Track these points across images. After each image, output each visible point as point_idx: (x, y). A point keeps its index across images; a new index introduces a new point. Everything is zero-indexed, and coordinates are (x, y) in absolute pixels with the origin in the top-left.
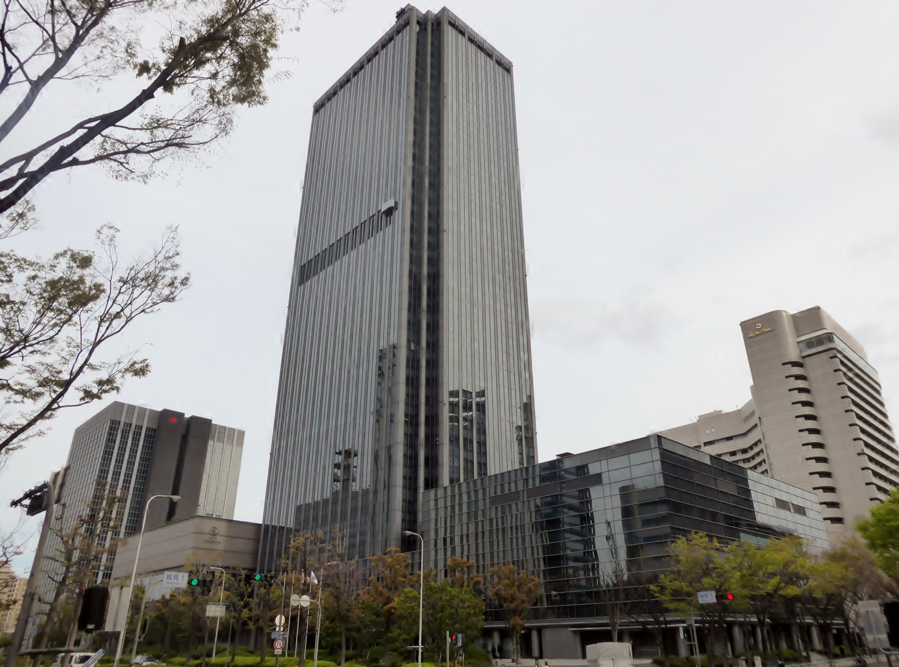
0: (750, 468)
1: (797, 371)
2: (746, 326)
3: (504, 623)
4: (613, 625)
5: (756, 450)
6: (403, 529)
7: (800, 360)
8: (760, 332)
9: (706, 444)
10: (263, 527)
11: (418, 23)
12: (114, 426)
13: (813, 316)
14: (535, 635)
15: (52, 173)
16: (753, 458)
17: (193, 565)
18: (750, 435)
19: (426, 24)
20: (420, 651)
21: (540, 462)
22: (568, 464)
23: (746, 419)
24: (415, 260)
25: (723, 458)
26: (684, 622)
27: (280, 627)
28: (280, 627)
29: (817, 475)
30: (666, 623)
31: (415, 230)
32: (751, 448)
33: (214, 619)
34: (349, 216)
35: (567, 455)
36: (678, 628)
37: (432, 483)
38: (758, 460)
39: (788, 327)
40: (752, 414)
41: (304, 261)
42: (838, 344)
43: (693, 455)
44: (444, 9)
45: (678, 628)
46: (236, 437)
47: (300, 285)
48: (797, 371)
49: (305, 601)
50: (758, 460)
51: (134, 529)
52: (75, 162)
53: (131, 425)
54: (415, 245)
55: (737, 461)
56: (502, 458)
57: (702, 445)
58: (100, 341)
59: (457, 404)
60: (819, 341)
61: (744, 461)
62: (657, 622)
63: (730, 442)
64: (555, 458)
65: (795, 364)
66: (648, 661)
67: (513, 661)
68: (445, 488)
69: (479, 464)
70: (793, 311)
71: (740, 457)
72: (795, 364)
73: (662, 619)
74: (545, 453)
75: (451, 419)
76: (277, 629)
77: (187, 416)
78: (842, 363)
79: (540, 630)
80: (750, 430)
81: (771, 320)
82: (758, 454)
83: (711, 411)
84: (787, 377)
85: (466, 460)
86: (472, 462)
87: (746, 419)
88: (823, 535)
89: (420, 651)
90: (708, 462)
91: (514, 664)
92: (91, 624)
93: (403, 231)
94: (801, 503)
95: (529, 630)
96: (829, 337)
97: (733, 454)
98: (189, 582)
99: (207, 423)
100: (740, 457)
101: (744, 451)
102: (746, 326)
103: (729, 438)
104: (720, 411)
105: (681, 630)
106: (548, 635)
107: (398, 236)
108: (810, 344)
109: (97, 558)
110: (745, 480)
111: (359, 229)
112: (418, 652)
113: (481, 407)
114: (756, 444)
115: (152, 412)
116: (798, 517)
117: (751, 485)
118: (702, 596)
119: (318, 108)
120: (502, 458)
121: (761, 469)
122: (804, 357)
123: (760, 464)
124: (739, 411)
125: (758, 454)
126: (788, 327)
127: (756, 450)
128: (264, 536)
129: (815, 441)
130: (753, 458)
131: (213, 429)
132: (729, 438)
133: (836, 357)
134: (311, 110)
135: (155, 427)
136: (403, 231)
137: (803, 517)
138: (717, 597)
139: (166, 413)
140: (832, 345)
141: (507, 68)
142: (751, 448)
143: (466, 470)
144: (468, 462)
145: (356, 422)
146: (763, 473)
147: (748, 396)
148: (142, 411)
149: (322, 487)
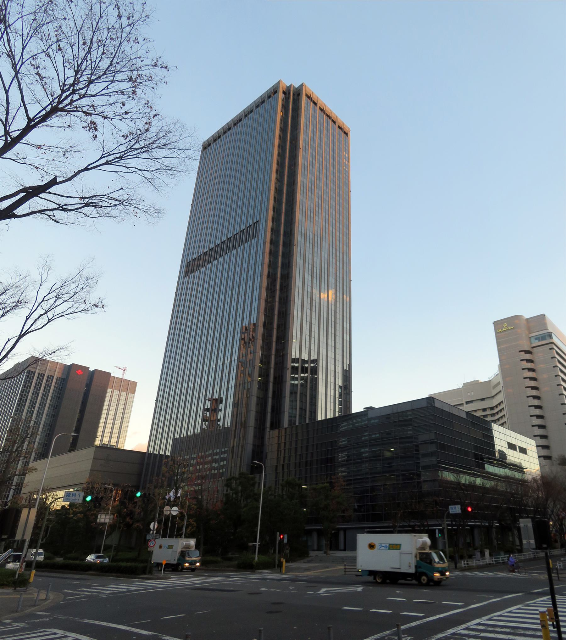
1: (528, 356)
6: (253, 459)
9: (467, 403)
10: (147, 455)
11: (284, 92)
14: (342, 534)
16: (497, 413)
17: (89, 483)
18: (496, 398)
19: (289, 94)
20: (257, 546)
21: (353, 412)
22: (371, 415)
23: (495, 387)
24: (272, 264)
26: (440, 525)
27: (153, 530)
29: (537, 427)
30: (429, 526)
31: (274, 243)
32: (496, 406)
33: (104, 524)
34: (225, 229)
35: (371, 408)
36: (435, 530)
37: (276, 424)
40: (499, 383)
41: (190, 259)
42: (555, 340)
43: (455, 412)
44: (302, 85)
45: (435, 530)
46: (129, 387)
47: (186, 276)
48: (528, 356)
49: (175, 511)
51: (43, 455)
52: (15, 216)
53: (44, 375)
54: (273, 253)
56: (327, 409)
57: (465, 404)
58: (25, 334)
59: (297, 367)
60: (543, 338)
63: (483, 402)
65: (527, 352)
67: (325, 553)
68: (286, 429)
69: (310, 411)
70: (527, 316)
72: (527, 352)
73: (425, 523)
74: (357, 407)
76: (151, 532)
77: (91, 369)
79: (345, 530)
80: (496, 394)
81: (514, 320)
82: (501, 411)
83: (472, 380)
85: (301, 409)
86: (306, 411)
87: (495, 387)
89: (257, 546)
90: (464, 416)
91: (325, 555)
92: (545, 544)
93: (265, 243)
94: (524, 446)
95: (339, 530)
96: (550, 335)
97: (484, 410)
99: (107, 375)
101: (492, 408)
103: (483, 400)
104: (478, 381)
105: (437, 531)
107: (260, 247)
108: (537, 338)
109: (11, 478)
110: (490, 430)
111: (232, 239)
112: (256, 547)
113: (315, 371)
114: (500, 404)
115: (66, 366)
116: (522, 455)
117: (495, 434)
118: (452, 509)
119: (206, 146)
120: (327, 409)
121: (502, 421)
122: (533, 348)
124: (489, 381)
127: (500, 408)
128: (143, 464)
129: (538, 414)
130: (497, 413)
131: (111, 379)
132: (483, 400)
133: (553, 349)
134: (200, 148)
135: (64, 377)
136: (265, 243)
137: (525, 455)
138: (461, 509)
139: (73, 367)
140: (551, 341)
141: (346, 134)
143: (301, 416)
144: (303, 410)
145: (222, 380)
149: (194, 426)
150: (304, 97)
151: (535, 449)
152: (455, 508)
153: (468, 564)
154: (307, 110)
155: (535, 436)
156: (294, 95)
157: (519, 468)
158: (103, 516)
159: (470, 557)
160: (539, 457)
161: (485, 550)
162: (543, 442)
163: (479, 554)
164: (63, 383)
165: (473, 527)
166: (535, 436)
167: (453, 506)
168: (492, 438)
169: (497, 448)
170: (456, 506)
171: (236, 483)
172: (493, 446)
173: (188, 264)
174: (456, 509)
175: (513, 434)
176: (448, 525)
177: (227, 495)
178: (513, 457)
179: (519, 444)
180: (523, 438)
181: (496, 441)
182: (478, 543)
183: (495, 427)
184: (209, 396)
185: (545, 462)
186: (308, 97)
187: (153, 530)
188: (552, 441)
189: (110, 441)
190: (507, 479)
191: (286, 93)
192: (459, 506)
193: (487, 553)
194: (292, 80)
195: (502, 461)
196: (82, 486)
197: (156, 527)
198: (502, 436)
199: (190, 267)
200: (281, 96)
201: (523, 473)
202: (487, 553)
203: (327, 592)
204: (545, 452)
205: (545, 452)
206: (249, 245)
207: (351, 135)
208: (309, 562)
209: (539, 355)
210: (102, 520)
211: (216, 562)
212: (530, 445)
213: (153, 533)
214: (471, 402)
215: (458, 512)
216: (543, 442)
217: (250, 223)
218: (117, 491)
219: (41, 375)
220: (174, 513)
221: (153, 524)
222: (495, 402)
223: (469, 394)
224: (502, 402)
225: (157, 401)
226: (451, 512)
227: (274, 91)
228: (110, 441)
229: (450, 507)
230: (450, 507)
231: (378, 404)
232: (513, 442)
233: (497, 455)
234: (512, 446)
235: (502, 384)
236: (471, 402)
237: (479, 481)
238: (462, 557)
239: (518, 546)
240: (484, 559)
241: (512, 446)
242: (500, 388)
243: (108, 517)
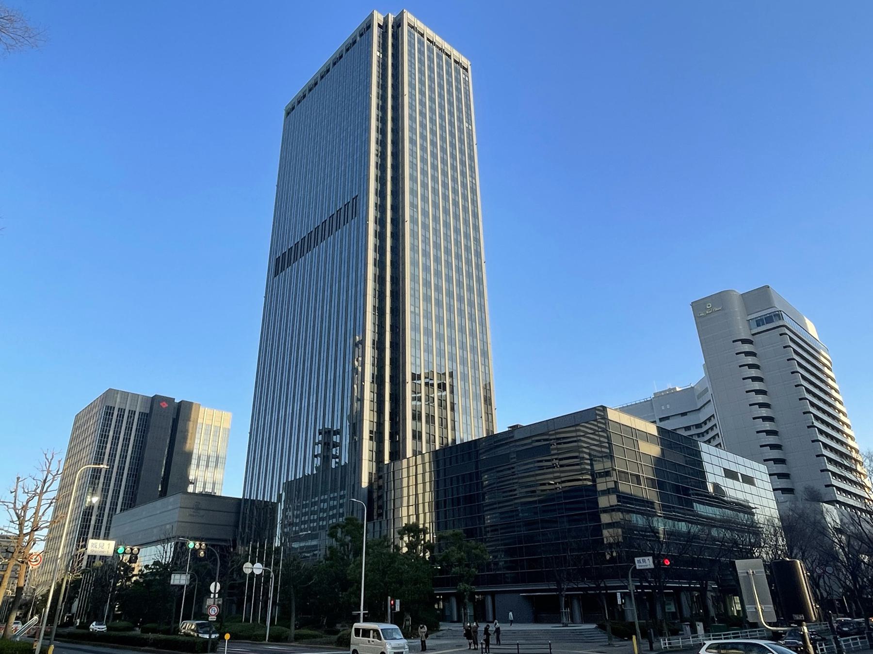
0: (705, 442)
1: (747, 348)
2: (697, 306)
3: (321, 601)
4: (560, 590)
5: (709, 425)
7: (751, 338)
8: (709, 313)
12: (109, 412)
13: (763, 294)
15: (524, 424)
16: (707, 432)
19: (387, 26)
22: (517, 436)
25: (678, 432)
27: (215, 594)
28: (215, 594)
30: (607, 588)
32: (705, 423)
38: (711, 434)
39: (737, 307)
40: (706, 390)
41: (279, 254)
42: (787, 321)
48: (747, 348)
50: (711, 434)
55: (692, 436)
60: (769, 319)
61: (698, 435)
62: (598, 587)
65: (744, 341)
66: (594, 626)
71: (694, 431)
72: (744, 341)
73: (602, 585)
74: (500, 427)
75: (414, 399)
76: (212, 596)
77: (177, 401)
78: (792, 339)
79: (493, 594)
81: (721, 298)
82: (712, 428)
84: (734, 341)
88: (773, 504)
97: (688, 428)
98: (116, 551)
100: (694, 431)
101: (698, 426)
102: (697, 306)
105: (619, 595)
106: (498, 598)
108: (759, 323)
110: (698, 453)
114: (709, 419)
115: (145, 398)
117: (705, 457)
122: (753, 335)
123: (714, 437)
125: (712, 428)
126: (737, 307)
127: (709, 425)
129: (769, 429)
130: (707, 432)
135: (148, 411)
138: (654, 562)
140: (781, 323)
142: (705, 423)
146: (716, 446)
147: (701, 374)
148: (135, 396)
149: (305, 464)
150: (406, 28)
151: (767, 478)
152: (644, 561)
153: (670, 644)
155: (765, 460)
156: (393, 27)
157: (745, 508)
158: (177, 576)
159: (675, 632)
160: (774, 490)
161: (697, 623)
162: (779, 469)
163: (688, 628)
164: (146, 419)
165: (678, 591)
166: (765, 460)
167: (641, 559)
168: (700, 463)
169: (711, 479)
170: (646, 558)
171: (342, 532)
172: (702, 474)
174: (645, 563)
175: (731, 456)
176: (637, 587)
177: (330, 548)
178: (734, 491)
179: (741, 470)
180: (748, 462)
181: (707, 467)
182: (686, 613)
183: (704, 447)
184: (319, 426)
185: (783, 497)
188: (794, 467)
189: (204, 488)
190: (725, 524)
192: (651, 558)
193: (700, 627)
195: (718, 498)
196: (742, 615)
197: (218, 588)
198: (715, 461)
199: (280, 264)
201: (753, 514)
202: (700, 627)
204: (783, 483)
205: (783, 483)
208: (438, 638)
209: (767, 345)
210: (177, 582)
211: (315, 637)
212: (760, 472)
214: (667, 418)
215: (648, 567)
216: (779, 469)
217: (348, 199)
219: (121, 411)
220: (257, 572)
221: (214, 584)
222: (702, 417)
223: (663, 408)
224: (713, 416)
225: (250, 433)
226: (638, 568)
228: (204, 488)
229: (636, 559)
230: (636, 559)
231: (526, 421)
232: (733, 468)
233: (710, 489)
234: (730, 474)
235: (710, 391)
236: (667, 418)
237: (683, 527)
238: (660, 633)
239: (663, 609)
240: (697, 637)
241: (730, 474)
242: (708, 396)
243: (184, 577)
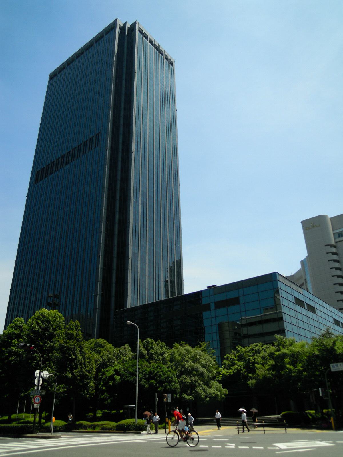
44: (135, 23)
64: (206, 288)
76: (36, 388)
83: (184, 278)
118: (333, 366)
141: (172, 64)
150: (137, 32)
152: (337, 366)
154: (140, 43)
167: (335, 364)
173: (38, 172)
186: (141, 31)
187: (38, 386)
191: (123, 28)
194: (126, 19)
200: (118, 31)
203: (245, 415)
206: (42, 182)
207: (175, 64)
213: (38, 388)
218: (40, 327)
227: (112, 27)
229: (331, 365)
230: (331, 365)
